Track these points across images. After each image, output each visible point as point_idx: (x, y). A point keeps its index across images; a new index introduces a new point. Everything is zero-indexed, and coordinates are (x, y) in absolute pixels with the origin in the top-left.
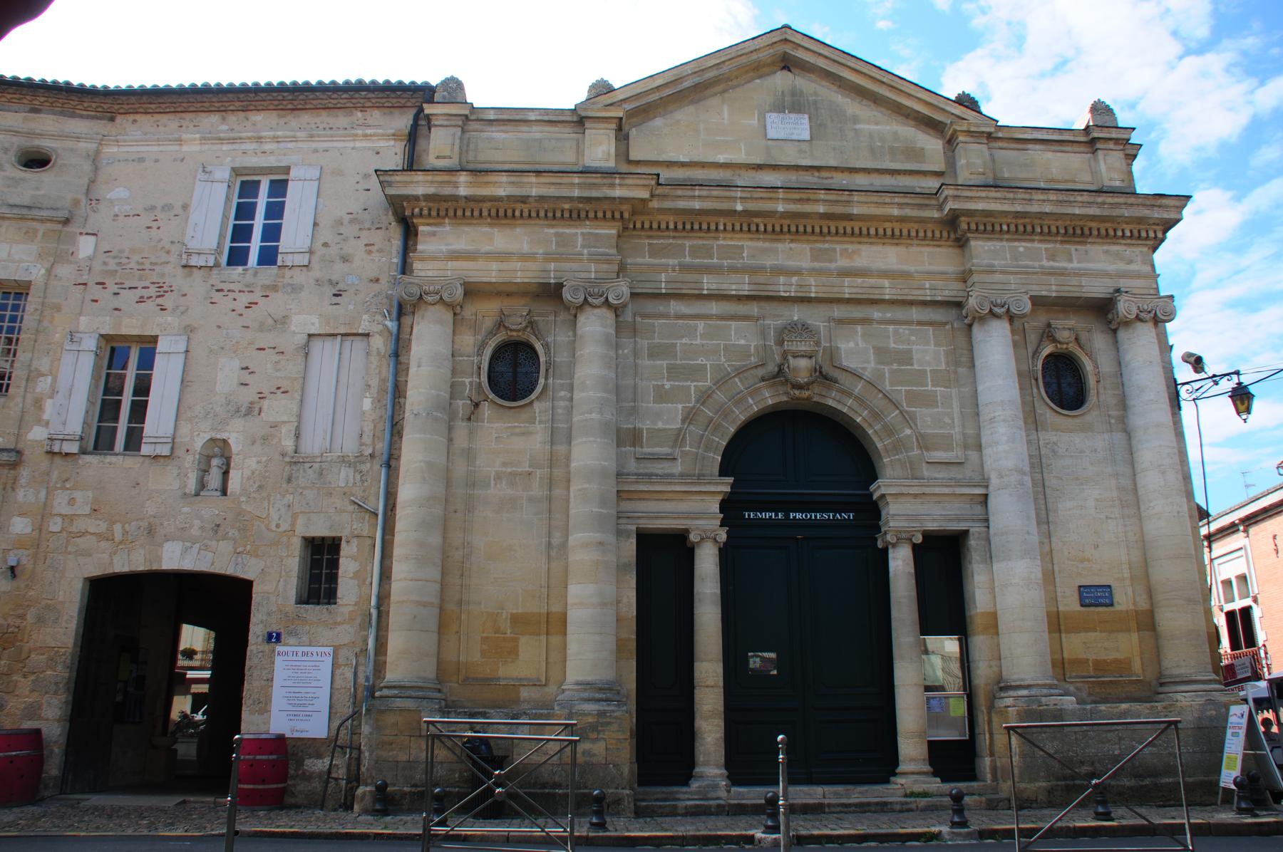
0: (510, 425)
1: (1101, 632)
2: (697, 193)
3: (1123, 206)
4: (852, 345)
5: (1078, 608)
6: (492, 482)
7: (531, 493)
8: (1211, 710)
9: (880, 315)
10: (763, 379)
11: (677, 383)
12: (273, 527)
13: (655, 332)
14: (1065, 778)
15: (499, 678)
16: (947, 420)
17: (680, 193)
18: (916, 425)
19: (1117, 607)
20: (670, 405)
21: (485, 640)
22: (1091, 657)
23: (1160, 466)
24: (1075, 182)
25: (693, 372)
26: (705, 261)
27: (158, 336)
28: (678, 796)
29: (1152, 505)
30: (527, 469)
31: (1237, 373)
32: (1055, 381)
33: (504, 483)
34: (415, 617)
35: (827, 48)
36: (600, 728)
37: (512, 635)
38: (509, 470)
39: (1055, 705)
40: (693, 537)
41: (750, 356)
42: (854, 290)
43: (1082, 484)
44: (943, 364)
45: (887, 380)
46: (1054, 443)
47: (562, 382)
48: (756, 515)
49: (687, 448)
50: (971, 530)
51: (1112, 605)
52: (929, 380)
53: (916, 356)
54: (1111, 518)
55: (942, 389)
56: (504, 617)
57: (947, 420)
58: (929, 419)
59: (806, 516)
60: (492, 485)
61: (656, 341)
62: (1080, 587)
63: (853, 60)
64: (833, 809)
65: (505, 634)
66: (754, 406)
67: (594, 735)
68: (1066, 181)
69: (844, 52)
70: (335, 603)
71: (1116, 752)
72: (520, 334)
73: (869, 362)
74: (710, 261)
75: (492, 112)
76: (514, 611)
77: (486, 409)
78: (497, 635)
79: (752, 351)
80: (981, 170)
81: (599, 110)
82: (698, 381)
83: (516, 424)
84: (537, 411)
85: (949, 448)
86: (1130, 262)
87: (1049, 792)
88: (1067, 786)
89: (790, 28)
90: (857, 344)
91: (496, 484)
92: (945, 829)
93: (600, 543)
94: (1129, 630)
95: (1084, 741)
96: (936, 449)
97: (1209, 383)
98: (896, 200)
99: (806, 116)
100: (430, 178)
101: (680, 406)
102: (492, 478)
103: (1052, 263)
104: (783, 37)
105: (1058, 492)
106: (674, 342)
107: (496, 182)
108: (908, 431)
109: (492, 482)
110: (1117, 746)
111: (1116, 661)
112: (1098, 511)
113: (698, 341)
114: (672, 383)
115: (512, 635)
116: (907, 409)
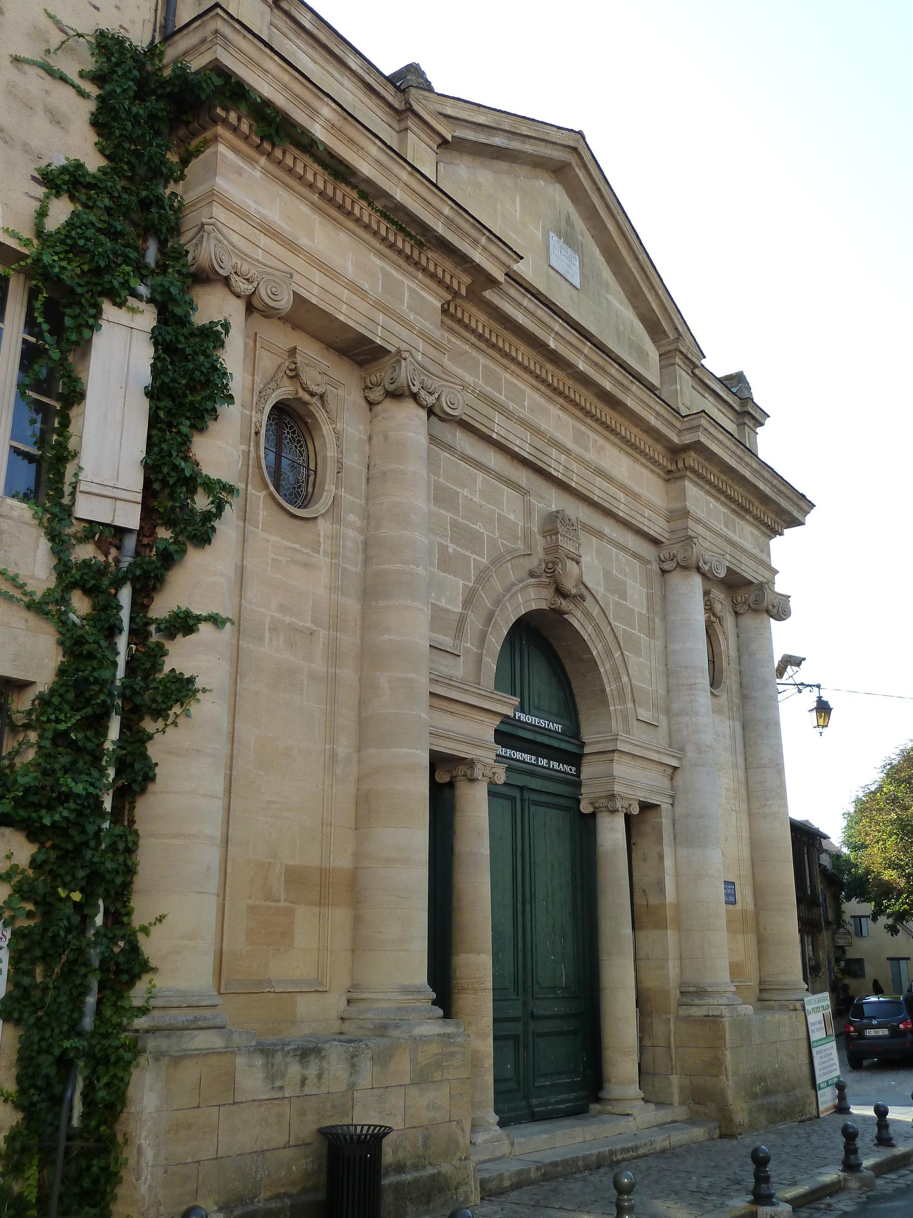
0: (289, 544)
6: (267, 635)
10: (532, 575)
13: (440, 467)
15: (270, 981)
21: (252, 909)
26: (489, 388)
29: (768, 803)
30: (308, 625)
31: (818, 686)
35: (607, 187)
37: (287, 904)
38: (288, 619)
47: (352, 499)
56: (277, 872)
60: (267, 641)
65: (278, 901)
66: (534, 606)
67: (437, 1076)
69: (500, 111)
75: (309, 15)
76: (291, 863)
78: (267, 903)
81: (430, 113)
83: (297, 546)
89: (583, 138)
91: (271, 639)
97: (794, 689)
100: (286, 78)
102: (267, 627)
104: (572, 144)
107: (362, 148)
109: (267, 635)
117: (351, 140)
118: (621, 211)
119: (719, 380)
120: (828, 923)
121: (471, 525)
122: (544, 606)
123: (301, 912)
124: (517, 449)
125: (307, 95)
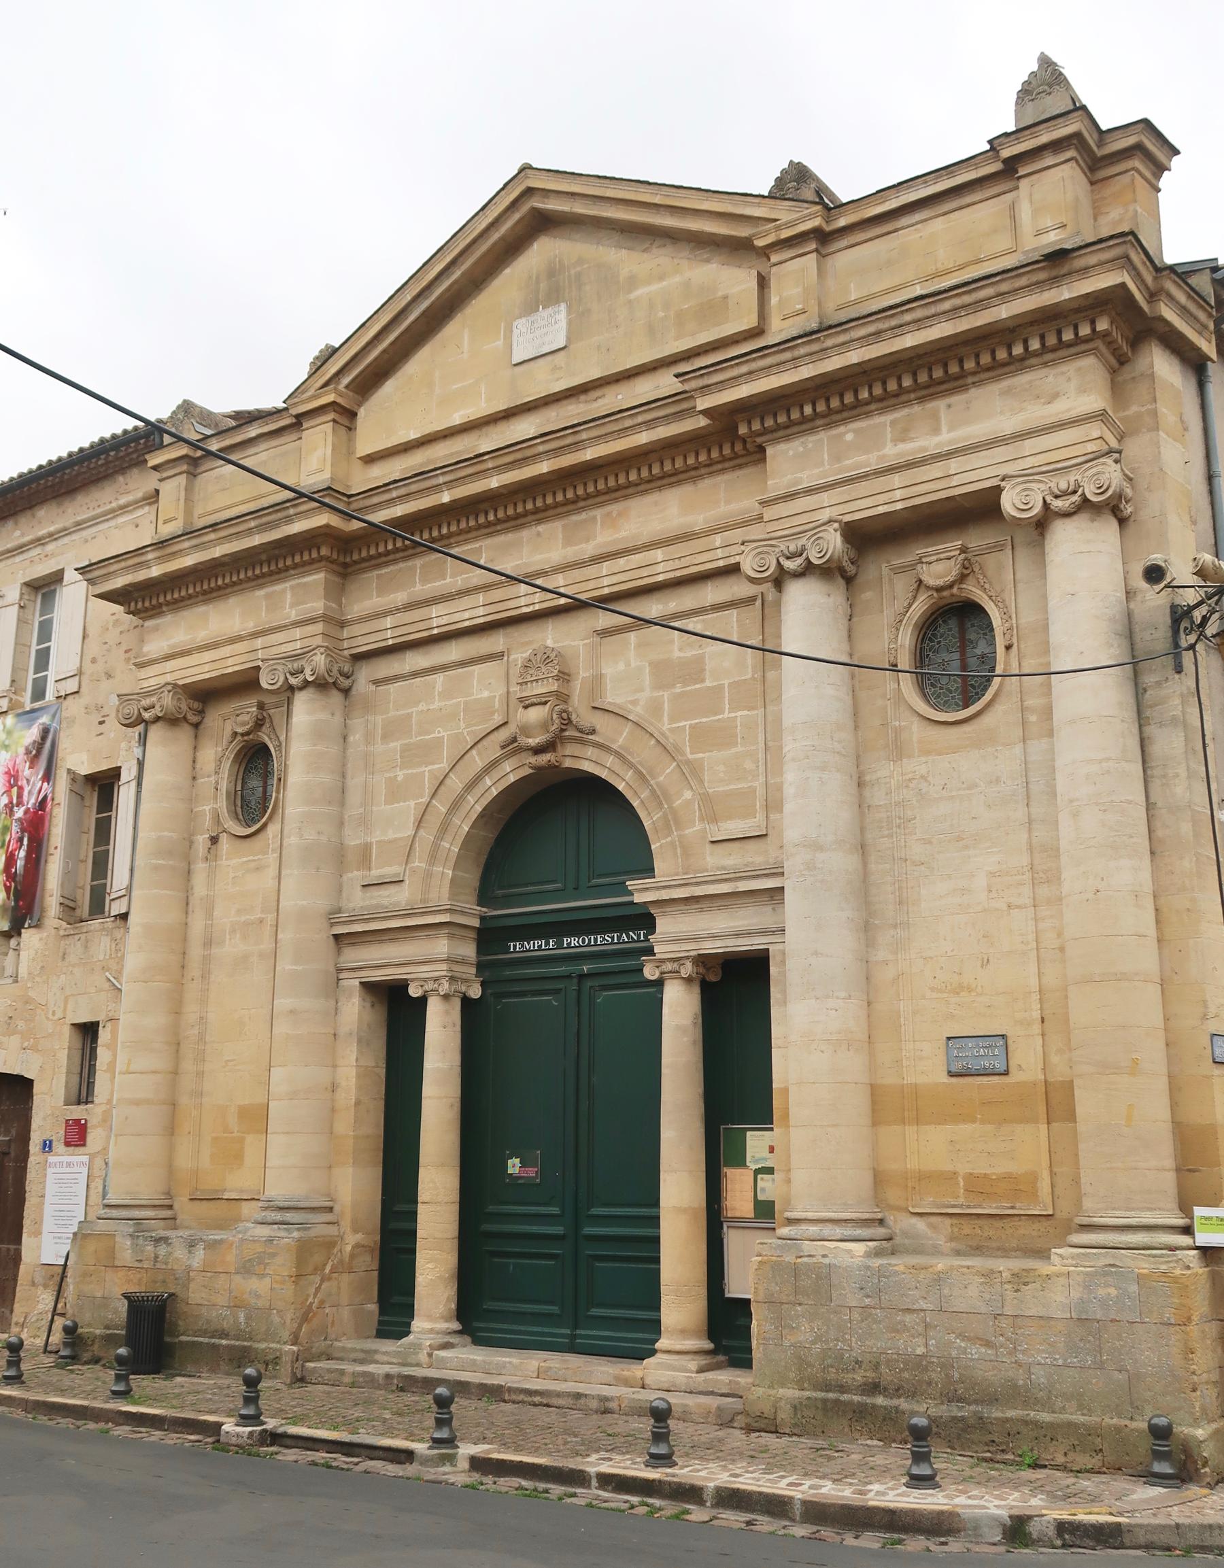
0: (245, 859)
1: (983, 1122)
2: (394, 494)
3: (996, 301)
4: (621, 666)
5: (944, 1078)
7: (262, 946)
8: (1107, 1285)
9: (660, 607)
11: (410, 771)
12: (50, 1016)
14: (827, 1387)
16: (749, 765)
17: (375, 500)
18: (701, 781)
19: (1016, 1076)
20: (402, 804)
22: (963, 1168)
23: (1071, 801)
24: (979, 261)
25: (427, 751)
27: (120, 767)
28: (377, 1357)
32: (956, 656)
33: (238, 936)
34: (127, 1118)
36: (267, 1261)
37: (239, 1134)
38: (243, 919)
39: (824, 1256)
40: (414, 991)
41: (493, 713)
42: (615, 579)
43: (967, 847)
44: (750, 670)
45: (666, 715)
46: (922, 777)
48: (523, 946)
49: (417, 864)
50: (771, 948)
51: (1006, 1073)
52: (727, 702)
53: (709, 665)
54: (1018, 907)
55: (746, 712)
57: (749, 765)
58: (722, 768)
59: (584, 941)
61: (392, 714)
62: (949, 1038)
63: (612, 184)
64: (514, 1397)
66: (492, 787)
68: (962, 267)
69: (599, 177)
70: (92, 1102)
71: (919, 1351)
72: (251, 737)
73: (642, 690)
74: (442, 582)
77: (225, 842)
79: (497, 703)
80: (799, 307)
82: (433, 764)
83: (251, 858)
84: (271, 837)
85: (749, 813)
86: (1054, 396)
87: (795, 1407)
88: (825, 1401)
90: (628, 664)
92: (420, 1447)
93: (291, 1011)
94: (1035, 1120)
95: (863, 1325)
96: (730, 818)
98: (640, 419)
99: (563, 307)
100: (123, 564)
101: (412, 803)
103: (902, 447)
105: (922, 868)
106: (410, 711)
108: (688, 795)
109: (228, 937)
110: (920, 1340)
111: (1008, 1177)
112: (994, 894)
113: (436, 705)
114: (405, 772)
115: (239, 1134)
116: (690, 757)
117: (174, 553)
118: (460, 234)
119: (771, 196)
120: (574, 1337)
121: (427, 737)
122: (527, 771)
123: (250, 1139)
124: (467, 624)
125: (137, 560)
